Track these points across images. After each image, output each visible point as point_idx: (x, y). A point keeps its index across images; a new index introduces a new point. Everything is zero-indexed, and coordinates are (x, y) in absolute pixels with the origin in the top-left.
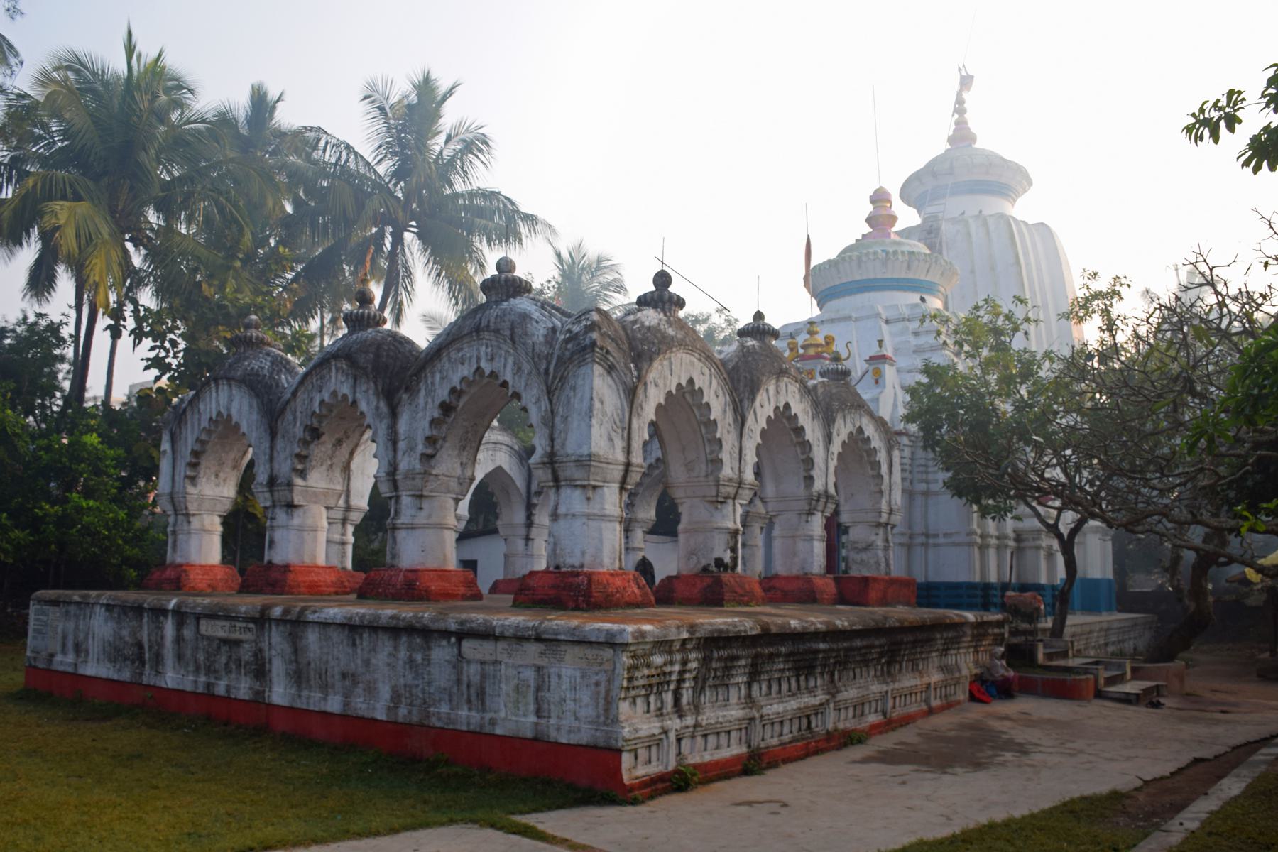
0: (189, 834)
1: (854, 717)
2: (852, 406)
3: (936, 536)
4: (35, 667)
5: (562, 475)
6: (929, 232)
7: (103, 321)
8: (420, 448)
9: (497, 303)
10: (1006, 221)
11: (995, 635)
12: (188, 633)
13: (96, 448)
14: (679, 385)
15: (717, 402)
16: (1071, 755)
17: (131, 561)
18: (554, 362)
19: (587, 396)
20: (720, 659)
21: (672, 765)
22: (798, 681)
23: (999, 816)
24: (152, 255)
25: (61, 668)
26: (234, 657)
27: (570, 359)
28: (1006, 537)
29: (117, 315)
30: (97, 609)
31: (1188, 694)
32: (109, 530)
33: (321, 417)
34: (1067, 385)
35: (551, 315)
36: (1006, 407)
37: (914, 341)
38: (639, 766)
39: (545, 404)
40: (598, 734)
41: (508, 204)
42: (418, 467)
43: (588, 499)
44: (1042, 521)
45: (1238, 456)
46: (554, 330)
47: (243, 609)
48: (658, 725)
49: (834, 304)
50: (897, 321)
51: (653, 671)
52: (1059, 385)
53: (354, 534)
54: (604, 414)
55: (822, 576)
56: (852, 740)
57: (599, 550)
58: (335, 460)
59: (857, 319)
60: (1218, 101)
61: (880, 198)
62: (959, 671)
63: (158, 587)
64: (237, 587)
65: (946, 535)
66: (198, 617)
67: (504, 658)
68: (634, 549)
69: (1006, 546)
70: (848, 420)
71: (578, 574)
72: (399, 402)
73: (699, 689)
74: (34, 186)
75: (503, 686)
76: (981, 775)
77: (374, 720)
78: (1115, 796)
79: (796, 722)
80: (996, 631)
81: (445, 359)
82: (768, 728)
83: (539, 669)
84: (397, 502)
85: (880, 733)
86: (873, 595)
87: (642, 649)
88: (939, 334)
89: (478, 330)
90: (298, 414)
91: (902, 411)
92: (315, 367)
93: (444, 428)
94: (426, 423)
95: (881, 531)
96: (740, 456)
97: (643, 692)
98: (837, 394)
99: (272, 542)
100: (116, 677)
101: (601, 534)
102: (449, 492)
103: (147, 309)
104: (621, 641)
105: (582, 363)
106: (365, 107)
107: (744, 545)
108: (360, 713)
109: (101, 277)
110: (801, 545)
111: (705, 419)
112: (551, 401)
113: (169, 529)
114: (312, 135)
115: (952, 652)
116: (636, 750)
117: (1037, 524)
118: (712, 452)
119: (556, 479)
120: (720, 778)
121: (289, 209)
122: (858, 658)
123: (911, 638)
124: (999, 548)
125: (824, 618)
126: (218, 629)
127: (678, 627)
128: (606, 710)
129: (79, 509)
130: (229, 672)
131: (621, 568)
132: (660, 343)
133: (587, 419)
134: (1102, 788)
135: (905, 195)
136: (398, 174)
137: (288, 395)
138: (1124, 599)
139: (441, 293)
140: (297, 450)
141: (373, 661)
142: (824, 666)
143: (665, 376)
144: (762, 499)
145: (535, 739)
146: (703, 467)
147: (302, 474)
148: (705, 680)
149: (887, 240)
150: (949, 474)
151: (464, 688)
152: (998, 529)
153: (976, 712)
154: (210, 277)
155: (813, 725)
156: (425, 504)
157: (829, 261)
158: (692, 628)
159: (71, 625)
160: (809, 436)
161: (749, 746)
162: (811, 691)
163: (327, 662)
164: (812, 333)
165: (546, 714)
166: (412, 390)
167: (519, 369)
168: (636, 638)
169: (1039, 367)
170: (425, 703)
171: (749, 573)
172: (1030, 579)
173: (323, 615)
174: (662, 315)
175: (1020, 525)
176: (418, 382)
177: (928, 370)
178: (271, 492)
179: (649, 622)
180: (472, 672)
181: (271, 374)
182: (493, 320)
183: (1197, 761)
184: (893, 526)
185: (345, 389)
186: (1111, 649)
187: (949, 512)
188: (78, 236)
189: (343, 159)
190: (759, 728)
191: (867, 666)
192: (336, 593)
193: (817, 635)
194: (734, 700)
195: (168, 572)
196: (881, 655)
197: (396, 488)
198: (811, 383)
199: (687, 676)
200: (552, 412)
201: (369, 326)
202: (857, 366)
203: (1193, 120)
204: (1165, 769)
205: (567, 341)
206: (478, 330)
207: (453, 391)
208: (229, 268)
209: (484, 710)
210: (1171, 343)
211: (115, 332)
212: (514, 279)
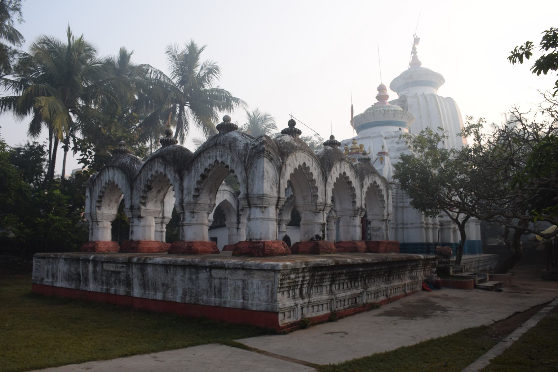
0: (101, 349)
2: (371, 173)
3: (407, 224)
5: (252, 203)
6: (402, 101)
7: (61, 145)
8: (193, 193)
9: (224, 134)
10: (434, 96)
12: (98, 269)
14: (300, 165)
15: (315, 172)
16: (465, 311)
17: (78, 240)
19: (262, 171)
20: (318, 275)
22: (351, 284)
23: (435, 336)
24: (80, 118)
25: (47, 284)
28: (436, 224)
29: (66, 142)
30: (61, 260)
31: (513, 286)
33: (151, 181)
34: (461, 163)
35: (246, 138)
36: (435, 172)
37: (397, 146)
38: (286, 319)
39: (244, 174)
43: (263, 212)
45: (532, 190)
46: (247, 144)
47: (121, 259)
48: (293, 302)
49: (361, 132)
50: (390, 138)
51: (291, 281)
52: (457, 163)
53: (166, 228)
54: (269, 178)
55: (360, 241)
60: (522, 46)
61: (381, 88)
62: (418, 278)
63: (86, 251)
65: (411, 224)
66: (102, 263)
68: (282, 232)
69: (436, 228)
71: (259, 242)
73: (310, 287)
74: (31, 90)
75: (229, 288)
76: (427, 320)
77: (177, 303)
78: (483, 328)
79: (350, 300)
80: (433, 262)
81: (202, 157)
82: (339, 303)
83: (243, 281)
85: (385, 304)
87: (286, 272)
88: (407, 143)
89: (216, 145)
91: (392, 174)
92: (148, 161)
93: (203, 185)
94: (195, 183)
95: (384, 223)
96: (325, 193)
97: (287, 289)
98: (365, 167)
99: (132, 232)
100: (69, 287)
102: (205, 210)
103: (79, 139)
105: (259, 157)
106: (167, 56)
107: (327, 229)
108: (170, 300)
109: (60, 127)
110: (351, 229)
112: (246, 173)
113: (90, 227)
114: (145, 68)
116: (284, 313)
118: (314, 192)
121: (137, 98)
125: (361, 258)
126: (110, 267)
127: (301, 263)
128: (272, 297)
130: (115, 284)
136: (182, 83)
138: (486, 249)
140: (142, 195)
141: (175, 279)
144: (335, 211)
145: (243, 309)
146: (310, 198)
147: (144, 204)
148: (312, 284)
150: (412, 199)
151: (213, 289)
152: (433, 221)
153: (425, 295)
154: (105, 126)
155: (358, 301)
156: (195, 215)
157: (361, 114)
158: (307, 263)
159: (50, 267)
161: (331, 310)
162: (356, 288)
163: (156, 279)
164: (354, 143)
166: (189, 170)
167: (233, 160)
169: (449, 155)
170: (197, 295)
173: (154, 261)
175: (442, 219)
176: (192, 166)
177: (402, 158)
178: (132, 212)
179: (289, 261)
180: (216, 282)
181: (131, 164)
182: (222, 141)
183: (517, 313)
184: (389, 221)
185: (161, 170)
186: (480, 269)
187: (412, 215)
188: (50, 111)
189: (159, 77)
190: (335, 303)
191: (380, 277)
192: (159, 252)
193: (358, 265)
194: (324, 292)
198: (354, 164)
199: (305, 282)
200: (247, 177)
201: (170, 144)
202: (373, 156)
203: (512, 54)
204: (504, 316)
205: (253, 149)
206: (216, 145)
207: (206, 169)
209: (221, 298)
210: (504, 145)
211: (66, 149)
212: (230, 124)
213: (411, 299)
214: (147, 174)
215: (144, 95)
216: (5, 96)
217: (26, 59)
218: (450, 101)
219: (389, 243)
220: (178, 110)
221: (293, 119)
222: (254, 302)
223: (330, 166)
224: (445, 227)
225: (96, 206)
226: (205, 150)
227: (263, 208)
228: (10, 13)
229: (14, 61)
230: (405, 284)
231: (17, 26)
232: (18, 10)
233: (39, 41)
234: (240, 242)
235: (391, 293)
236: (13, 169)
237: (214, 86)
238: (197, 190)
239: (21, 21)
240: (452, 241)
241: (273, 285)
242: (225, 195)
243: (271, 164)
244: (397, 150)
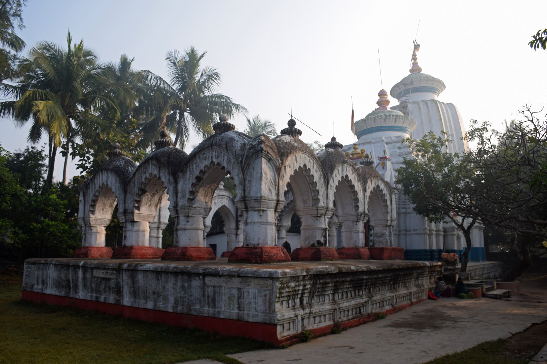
1: (379, 307)
2: (374, 176)
3: (410, 231)
4: (26, 290)
5: (249, 206)
6: (403, 107)
7: (59, 150)
8: (188, 196)
9: (220, 134)
10: (435, 102)
11: (438, 271)
12: (88, 275)
13: (55, 200)
14: (300, 167)
15: (316, 174)
17: (68, 243)
18: (245, 157)
19: (260, 171)
20: (320, 284)
21: (300, 331)
22: (355, 293)
23: (451, 352)
25: (36, 291)
26: (107, 285)
27: (252, 156)
28: (440, 231)
30: (51, 266)
31: (521, 295)
32: (61, 234)
33: (145, 184)
34: (465, 167)
35: (243, 138)
36: (439, 177)
37: (398, 151)
38: (285, 332)
39: (241, 176)
40: (266, 317)
41: (227, 99)
42: (187, 204)
44: (456, 223)
46: (244, 144)
47: (111, 265)
48: (293, 313)
49: (364, 137)
50: (391, 143)
51: (291, 290)
52: (461, 168)
53: (162, 234)
54: (267, 179)
55: (363, 247)
57: (266, 238)
58: (152, 202)
59: (374, 143)
61: (382, 94)
62: (424, 286)
65: (414, 230)
66: (92, 269)
67: (224, 285)
68: (282, 238)
69: (440, 234)
70: (373, 182)
71: (257, 248)
73: (311, 297)
74: (29, 95)
75: (223, 297)
77: (167, 312)
78: (501, 341)
79: (354, 310)
81: (198, 158)
82: (342, 313)
83: (239, 289)
85: (391, 314)
86: (385, 255)
90: (136, 183)
91: (394, 180)
95: (388, 228)
96: (327, 197)
97: (286, 299)
99: (125, 237)
100: (58, 294)
102: (200, 214)
103: (77, 144)
104: (276, 276)
105: (257, 157)
106: (167, 62)
107: (329, 235)
108: (161, 309)
110: (354, 235)
111: (311, 182)
113: (83, 232)
115: (420, 278)
116: (283, 325)
118: (315, 196)
121: (137, 104)
122: (381, 282)
124: (437, 235)
126: (100, 274)
127: (302, 270)
128: (270, 307)
129: (49, 226)
130: (105, 292)
131: (275, 245)
133: (259, 181)
134: (495, 338)
136: (182, 89)
137: (131, 175)
138: (489, 256)
139: (200, 136)
141: (167, 286)
144: (337, 216)
145: (238, 320)
146: (311, 202)
147: (138, 208)
148: (314, 293)
150: (415, 205)
151: (206, 298)
152: (436, 227)
154: (103, 131)
155: (362, 311)
156: (190, 220)
158: (308, 270)
159: (40, 273)
160: (356, 189)
161: (334, 321)
162: (361, 297)
164: (355, 149)
165: (242, 309)
166: (184, 172)
167: (230, 161)
168: (283, 275)
170: (189, 304)
171: (331, 247)
172: (450, 248)
173: (145, 267)
174: (292, 138)
175: (446, 225)
176: (186, 168)
177: (405, 162)
178: (125, 216)
179: (288, 268)
180: (210, 291)
181: (125, 167)
182: (218, 141)
183: (534, 325)
185: (156, 172)
186: (485, 276)
187: (415, 220)
188: (48, 115)
189: (158, 84)
190: (338, 313)
191: (385, 285)
192: (153, 258)
193: (363, 273)
194: (327, 301)
196: (391, 280)
198: (357, 167)
199: (306, 291)
200: (244, 179)
201: (165, 146)
202: (376, 161)
203: (534, 39)
205: (250, 149)
206: (211, 145)
207: (201, 171)
208: (111, 127)
210: (517, 144)
212: (227, 124)
213: (419, 309)
214: (141, 177)
215: (144, 102)
216: (4, 101)
217: (26, 64)
218: (451, 106)
219: (394, 249)
221: (293, 118)
222: (250, 312)
223: (332, 169)
225: (90, 211)
227: (261, 211)
228: (12, 18)
229: (15, 66)
230: (411, 293)
231: (18, 33)
232: (19, 16)
233: (39, 46)
234: (236, 248)
235: (396, 303)
236: (8, 175)
237: (215, 92)
238: (192, 193)
239: (21, 26)
240: (456, 248)
242: (224, 200)
243: (269, 164)
244: (399, 155)
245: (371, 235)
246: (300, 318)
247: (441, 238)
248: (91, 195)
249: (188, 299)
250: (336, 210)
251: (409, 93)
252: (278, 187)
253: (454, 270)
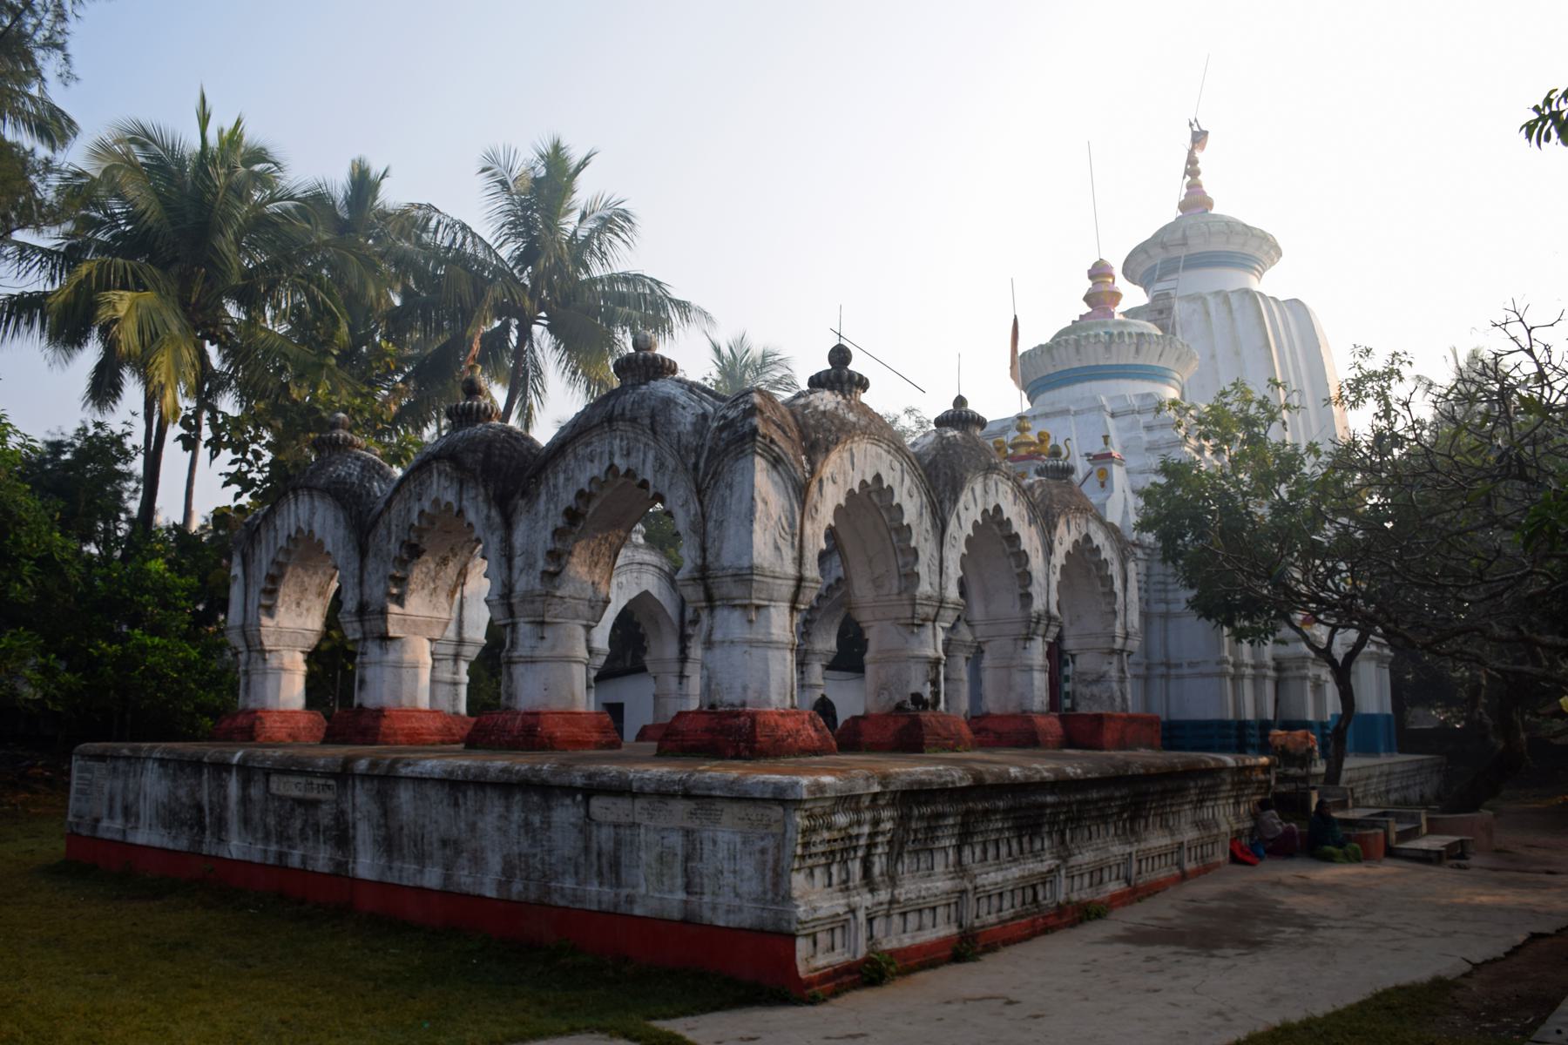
1: (1091, 885)
2: (1077, 509)
3: (1179, 666)
4: (78, 835)
5: (716, 593)
6: (1159, 310)
7: (174, 430)
8: (541, 564)
9: (634, 387)
11: (1260, 782)
12: (256, 792)
13: (162, 576)
14: (863, 482)
15: (911, 503)
17: (198, 700)
18: (705, 455)
19: (748, 495)
20: (921, 817)
21: (862, 952)
22: (1020, 843)
23: (1295, 1016)
24: (232, 352)
25: (108, 836)
26: (311, 821)
28: (1264, 666)
30: (150, 764)
31: (1498, 851)
32: (179, 672)
33: (421, 532)
34: (1338, 482)
35: (701, 398)
36: (1262, 511)
37: (1146, 437)
38: (819, 955)
39: (694, 507)
42: (538, 586)
44: (1311, 646)
46: (704, 416)
47: (322, 762)
48: (843, 902)
49: (1042, 398)
50: (1125, 414)
51: (836, 834)
52: (1324, 486)
54: (769, 516)
55: (1043, 714)
56: (1088, 913)
57: (765, 683)
58: (439, 583)
59: (1076, 413)
61: (1099, 272)
62: (1218, 826)
64: (321, 735)
65: (1191, 665)
66: (267, 773)
67: (643, 819)
68: (811, 686)
69: (1265, 677)
70: (1072, 527)
71: (738, 715)
72: (515, 510)
73: (895, 855)
74: (89, 275)
75: (642, 854)
77: (482, 898)
78: (1439, 986)
79: (1019, 893)
81: (570, 457)
82: (984, 902)
83: (688, 833)
84: (514, 630)
85: (1124, 904)
86: (1108, 735)
91: (1134, 519)
94: (548, 534)
95: (1115, 659)
96: (941, 569)
98: (1056, 487)
99: (362, 682)
100: (171, 846)
101: (767, 665)
102: (578, 617)
103: (225, 416)
106: (483, 180)
108: (465, 889)
110: (1018, 678)
111: (895, 524)
112: (701, 503)
113: (241, 668)
115: (1209, 803)
116: (814, 935)
117: (1304, 648)
118: (906, 565)
119: (709, 598)
120: (923, 967)
121: (397, 302)
123: (1159, 788)
124: (1257, 680)
125: (1051, 765)
127: (867, 779)
128: (776, 885)
129: (143, 649)
130: (305, 839)
132: (839, 430)
133: (747, 523)
135: (1128, 271)
136: (525, 258)
137: (381, 505)
138: (1406, 739)
139: (577, 394)
141: (480, 825)
142: (1052, 824)
143: (843, 472)
144: (969, 624)
145: (685, 921)
146: (895, 583)
148: (902, 845)
149: (1110, 321)
151: (594, 857)
152: (1254, 656)
154: (300, 377)
155: (1040, 897)
156: (548, 633)
157: (1041, 346)
158: (885, 779)
159: (119, 784)
161: (960, 926)
162: (1036, 855)
163: (424, 826)
164: (1022, 430)
166: (530, 496)
167: (662, 465)
169: (1302, 462)
170: (545, 876)
171: (952, 712)
172: (1294, 715)
173: (418, 769)
174: (840, 398)
175: (1283, 651)
176: (538, 485)
177: (1166, 469)
178: (361, 621)
180: (604, 837)
181: (361, 481)
182: (628, 407)
183: (1535, 937)
185: (449, 496)
186: (1393, 797)
187: (1194, 636)
188: (141, 332)
189: (459, 241)
190: (972, 902)
191: (1106, 823)
192: (443, 742)
193: (1043, 786)
194: (939, 868)
195: (239, 719)
196: (1123, 809)
197: (511, 614)
199: (880, 839)
200: (703, 516)
201: (478, 421)
203: (1536, 116)
205: (721, 429)
206: (610, 419)
207: (581, 494)
208: (322, 366)
210: (1486, 416)
211: (190, 443)
212: (655, 357)
215: (418, 294)
216: (16, 292)
218: (1296, 307)
219: (1132, 719)
220: (514, 337)
221: (844, 342)
222: (720, 900)
224: (1290, 674)
225: (260, 606)
226: (580, 433)
227: (752, 610)
228: (39, 55)
229: (48, 190)
231: (57, 95)
232: (61, 47)
234: (680, 715)
236: (26, 501)
238: (555, 556)
239: (67, 78)
240: (1310, 717)
241: (779, 847)
243: (775, 474)
245: (1067, 679)
246: (861, 915)
247: (1269, 688)
248: (264, 562)
249: (542, 860)
250: (967, 607)
251: (1176, 270)
252: (801, 541)
253: (1304, 779)
